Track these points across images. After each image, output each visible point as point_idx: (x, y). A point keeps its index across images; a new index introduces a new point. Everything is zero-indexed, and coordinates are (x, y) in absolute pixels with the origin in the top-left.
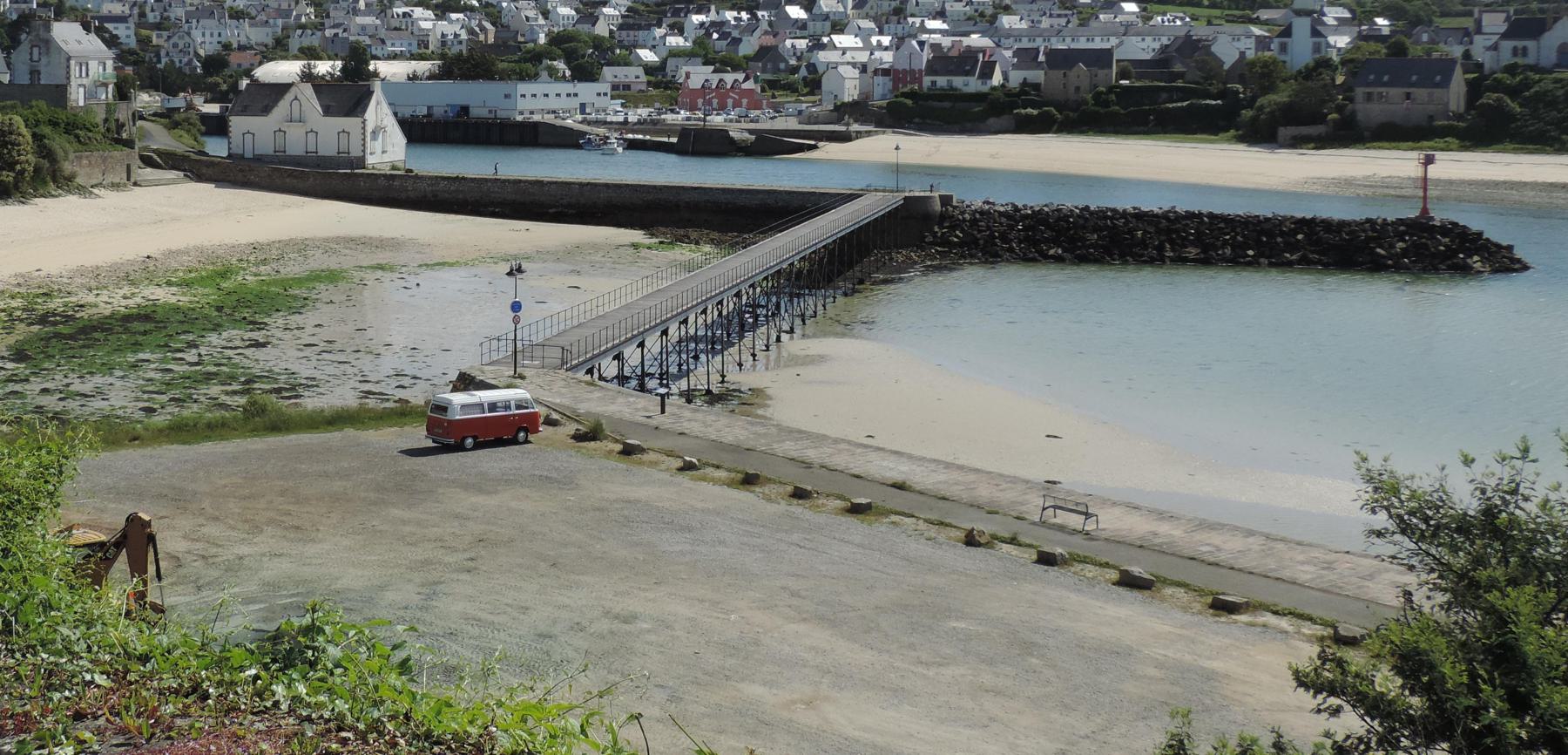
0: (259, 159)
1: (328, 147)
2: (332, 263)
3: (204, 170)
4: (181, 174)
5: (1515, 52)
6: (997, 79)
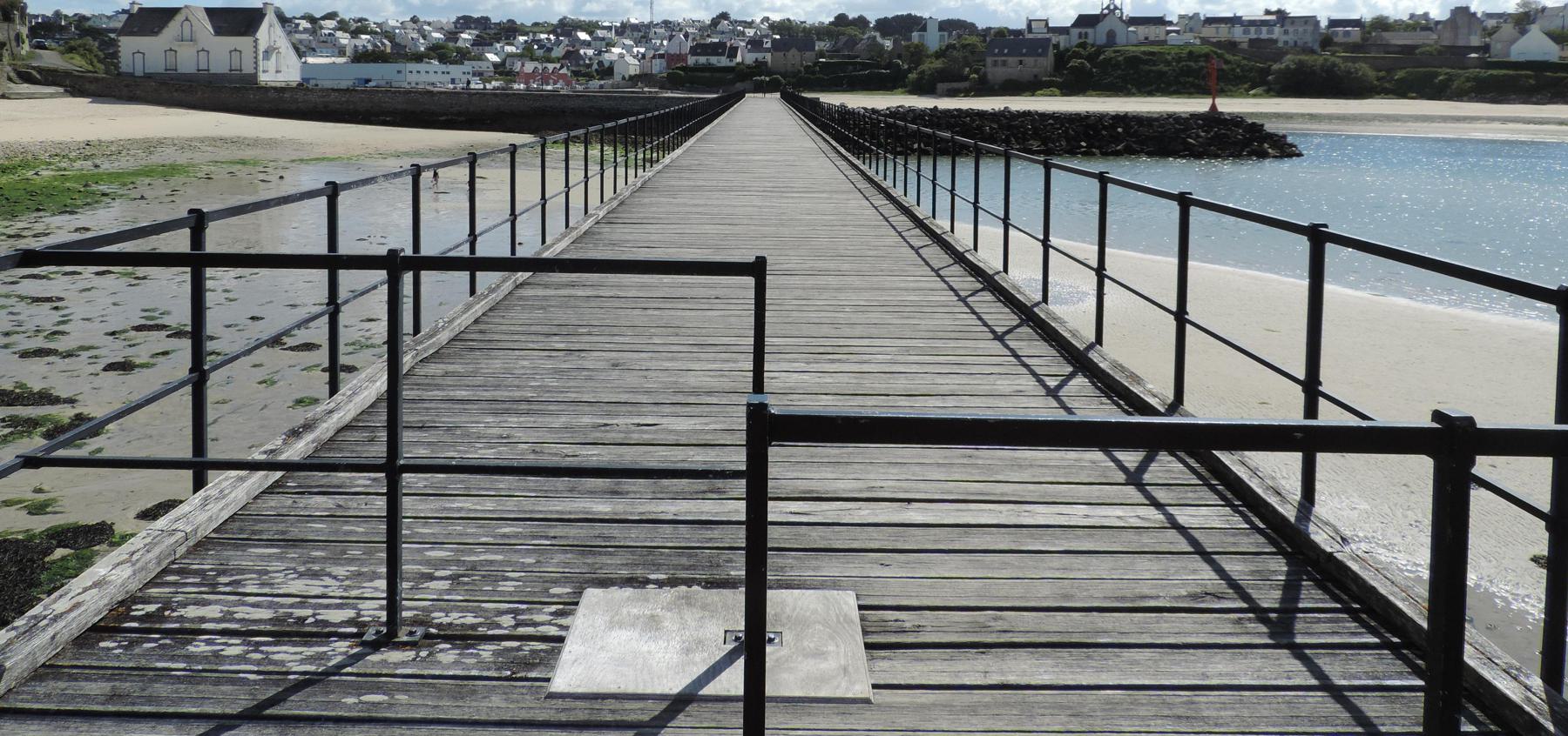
0: (149, 77)
1: (219, 65)
2: (182, 159)
3: (87, 86)
4: (61, 90)
5: (1080, 35)
6: (739, 59)
